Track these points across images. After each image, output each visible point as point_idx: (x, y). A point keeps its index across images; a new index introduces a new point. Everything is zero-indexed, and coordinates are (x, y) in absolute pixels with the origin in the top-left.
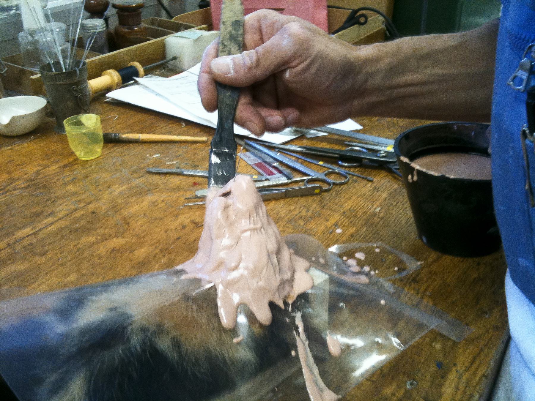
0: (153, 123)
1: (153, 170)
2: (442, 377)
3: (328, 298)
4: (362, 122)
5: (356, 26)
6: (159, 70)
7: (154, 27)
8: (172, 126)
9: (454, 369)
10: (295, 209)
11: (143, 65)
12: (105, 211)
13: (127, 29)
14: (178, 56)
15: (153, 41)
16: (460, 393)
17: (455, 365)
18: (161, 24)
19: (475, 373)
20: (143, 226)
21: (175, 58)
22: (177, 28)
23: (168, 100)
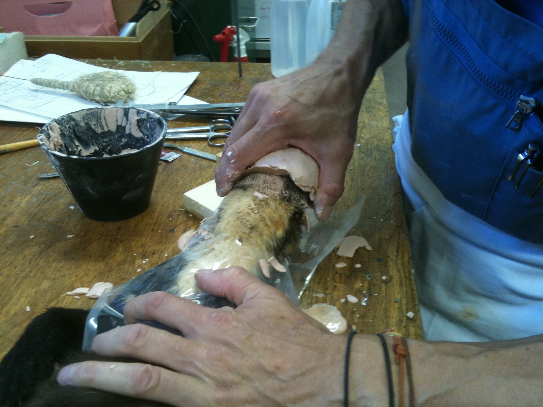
1: (45, 176)
2: (386, 266)
5: (151, 12)
8: (17, 132)
12: (26, 223)
16: (402, 272)
17: (388, 257)
23: (9, 108)
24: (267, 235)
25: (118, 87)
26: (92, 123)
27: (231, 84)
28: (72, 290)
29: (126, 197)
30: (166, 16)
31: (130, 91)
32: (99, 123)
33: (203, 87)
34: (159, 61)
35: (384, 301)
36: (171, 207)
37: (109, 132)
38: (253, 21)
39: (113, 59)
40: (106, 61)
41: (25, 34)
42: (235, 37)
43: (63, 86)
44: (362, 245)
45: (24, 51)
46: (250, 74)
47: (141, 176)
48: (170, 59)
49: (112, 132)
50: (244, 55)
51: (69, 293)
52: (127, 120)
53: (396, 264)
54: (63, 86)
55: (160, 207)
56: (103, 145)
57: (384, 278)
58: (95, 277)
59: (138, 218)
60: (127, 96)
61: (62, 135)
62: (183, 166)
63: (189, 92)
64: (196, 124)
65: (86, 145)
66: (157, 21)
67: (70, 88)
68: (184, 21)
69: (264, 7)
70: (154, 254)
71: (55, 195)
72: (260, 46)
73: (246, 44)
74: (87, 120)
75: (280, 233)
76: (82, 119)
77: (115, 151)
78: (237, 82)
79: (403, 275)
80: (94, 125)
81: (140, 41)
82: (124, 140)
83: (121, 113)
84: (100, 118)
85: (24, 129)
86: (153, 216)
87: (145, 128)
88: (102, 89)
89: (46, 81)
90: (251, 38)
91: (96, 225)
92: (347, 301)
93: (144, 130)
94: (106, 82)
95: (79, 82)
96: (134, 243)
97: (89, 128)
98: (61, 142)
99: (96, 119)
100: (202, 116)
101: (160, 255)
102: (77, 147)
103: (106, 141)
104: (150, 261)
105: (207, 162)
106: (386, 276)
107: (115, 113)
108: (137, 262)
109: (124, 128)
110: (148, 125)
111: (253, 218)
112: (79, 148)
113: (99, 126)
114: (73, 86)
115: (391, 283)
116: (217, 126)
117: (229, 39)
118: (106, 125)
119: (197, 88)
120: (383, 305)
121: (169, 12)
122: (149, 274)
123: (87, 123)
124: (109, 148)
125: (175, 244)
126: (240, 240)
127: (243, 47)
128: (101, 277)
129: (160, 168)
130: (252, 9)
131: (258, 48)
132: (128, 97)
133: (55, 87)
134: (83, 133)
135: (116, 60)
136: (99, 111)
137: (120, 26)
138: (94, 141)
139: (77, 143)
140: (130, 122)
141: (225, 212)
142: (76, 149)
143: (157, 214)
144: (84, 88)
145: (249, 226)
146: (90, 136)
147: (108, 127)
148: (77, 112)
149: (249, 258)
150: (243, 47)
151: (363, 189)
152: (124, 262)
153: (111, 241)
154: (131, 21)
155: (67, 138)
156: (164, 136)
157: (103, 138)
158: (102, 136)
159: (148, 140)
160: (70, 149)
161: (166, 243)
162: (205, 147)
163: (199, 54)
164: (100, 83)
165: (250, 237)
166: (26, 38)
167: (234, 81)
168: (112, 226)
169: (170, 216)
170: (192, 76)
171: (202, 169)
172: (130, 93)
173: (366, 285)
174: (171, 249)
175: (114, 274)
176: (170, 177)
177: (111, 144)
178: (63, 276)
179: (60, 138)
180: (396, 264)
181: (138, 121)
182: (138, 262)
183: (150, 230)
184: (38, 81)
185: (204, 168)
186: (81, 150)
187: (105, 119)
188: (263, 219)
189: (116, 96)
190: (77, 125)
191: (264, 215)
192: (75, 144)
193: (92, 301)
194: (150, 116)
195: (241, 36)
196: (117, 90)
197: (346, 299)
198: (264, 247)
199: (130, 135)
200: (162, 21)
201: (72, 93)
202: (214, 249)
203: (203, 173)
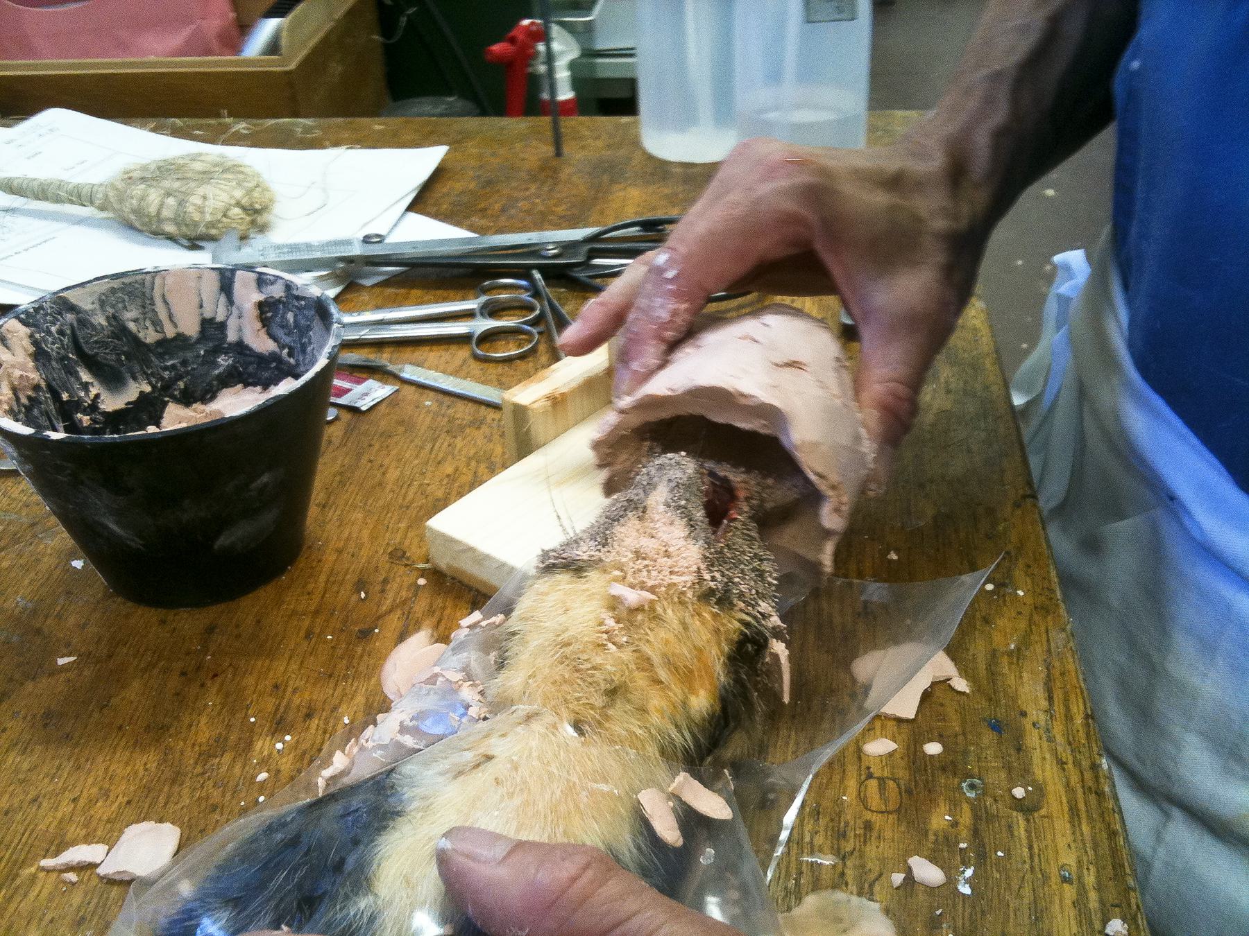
3: (529, 119)
4: (468, 222)
9: (1027, 723)
10: (457, 469)
13: (266, 485)
19: (1069, 717)
24: (662, 712)
25: (224, 197)
26: (130, 316)
27: (533, 178)
28: (57, 853)
29: (223, 541)
31: (257, 206)
32: (150, 315)
33: (458, 186)
34: (340, 120)
35: (1028, 876)
36: (364, 553)
37: (181, 339)
39: (218, 116)
42: (541, 47)
43: (79, 196)
44: (941, 675)
46: (583, 147)
47: (265, 478)
48: (374, 111)
50: (565, 94)
51: (48, 862)
52: (231, 302)
53: (1051, 740)
54: (79, 196)
55: (333, 557)
56: (162, 379)
57: (1019, 792)
58: (129, 802)
59: (265, 594)
60: (248, 219)
61: (40, 355)
62: (402, 423)
63: (422, 202)
64: (439, 292)
65: (113, 380)
67: (98, 202)
68: (410, 12)
70: (309, 716)
71: (33, 525)
72: (607, 68)
73: (572, 66)
74: (113, 306)
75: (701, 702)
76: (97, 306)
77: (198, 394)
78: (548, 172)
79: (1075, 779)
80: (136, 321)
82: (224, 361)
83: (211, 284)
84: (152, 299)
86: (310, 587)
87: (282, 327)
88: (181, 203)
90: (583, 50)
91: (144, 617)
92: (910, 879)
93: (280, 333)
94: (193, 184)
95: (120, 185)
96: (250, 681)
97: (120, 331)
98: (35, 376)
99: (139, 302)
100: (456, 271)
101: (327, 723)
102: (86, 386)
103: (173, 366)
104: (298, 742)
105: (471, 407)
106: (1024, 786)
108: (258, 745)
109: (222, 326)
110: (290, 316)
111: (613, 661)
112: (94, 391)
113: (148, 323)
114: (106, 197)
115: (1043, 812)
116: (497, 301)
117: (527, 55)
118: (170, 317)
119: (442, 189)
120: (1027, 892)
122: (279, 836)
123: (114, 317)
124: (181, 384)
125: (373, 681)
126: (577, 726)
127: (563, 75)
128: (146, 808)
129: (333, 433)
131: (602, 74)
132: (253, 222)
133: (58, 200)
135: (228, 120)
136: (148, 277)
137: (244, 28)
138: (137, 368)
139: (85, 376)
140: (238, 308)
141: (524, 642)
142: (82, 394)
143: (323, 578)
145: (603, 686)
146: (124, 353)
148: (82, 285)
149: (605, 788)
150: (563, 75)
151: (922, 486)
152: (218, 746)
153: (183, 674)
154: (270, 14)
155: (54, 363)
156: (333, 358)
157: (161, 356)
159: (292, 361)
160: (65, 396)
161: (346, 677)
162: (465, 361)
163: (450, 95)
164: (177, 185)
165: (607, 718)
167: (542, 169)
168: (188, 622)
169: (360, 585)
170: (422, 161)
171: (454, 429)
172: (257, 212)
173: (966, 818)
174: (360, 699)
175: (186, 792)
176: (364, 460)
177: (187, 373)
178: (35, 800)
179: (31, 364)
180: (1051, 740)
181: (261, 306)
182: (262, 746)
183: (302, 634)
184: (15, 183)
185: (462, 428)
186: (97, 396)
187: (165, 302)
188: (645, 663)
189: (219, 221)
190: (83, 322)
191: (647, 650)
192: (78, 378)
193: (115, 892)
194: (295, 292)
195: (556, 46)
196: (220, 205)
197: (909, 871)
198: (652, 751)
199: (240, 348)
201: (104, 215)
202: (489, 758)
203: (459, 442)
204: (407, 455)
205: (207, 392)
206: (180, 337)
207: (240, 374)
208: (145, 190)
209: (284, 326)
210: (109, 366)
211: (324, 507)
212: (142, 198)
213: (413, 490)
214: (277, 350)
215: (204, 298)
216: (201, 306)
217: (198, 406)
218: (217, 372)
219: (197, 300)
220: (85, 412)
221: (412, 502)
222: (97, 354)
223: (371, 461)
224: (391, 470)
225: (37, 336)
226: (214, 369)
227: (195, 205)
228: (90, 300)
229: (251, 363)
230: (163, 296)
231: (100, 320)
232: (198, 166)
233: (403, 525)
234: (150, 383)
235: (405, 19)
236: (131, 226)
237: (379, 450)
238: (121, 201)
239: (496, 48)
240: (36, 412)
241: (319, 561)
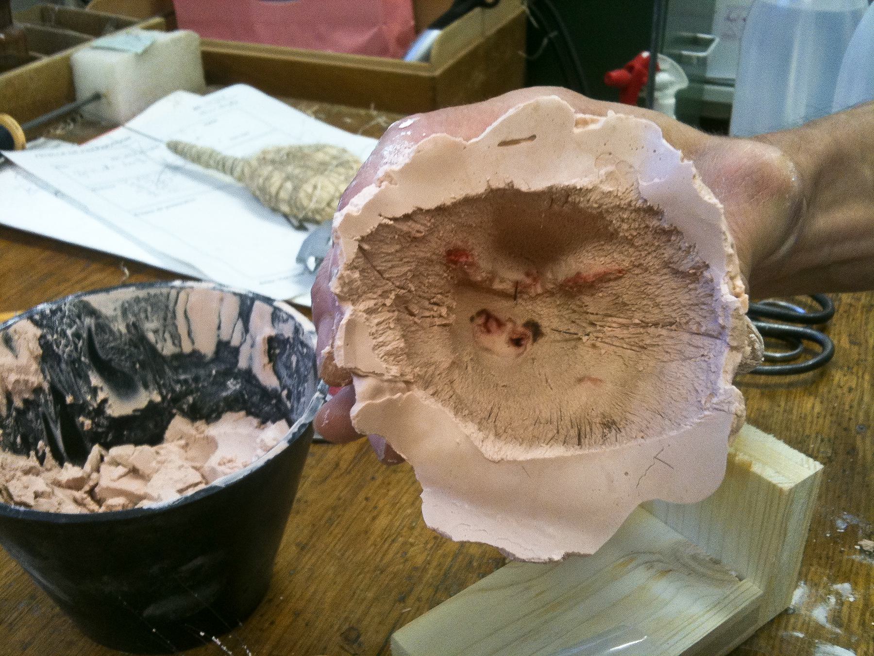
0: (50, 274)
5: (477, 10)
6: (62, 125)
7: (48, 29)
11: (21, 121)
14: (102, 90)
15: (45, 60)
18: (63, 20)
20: (30, 643)
21: (97, 97)
22: (97, 28)
25: (331, 189)
26: (150, 327)
30: (515, 21)
32: (170, 328)
37: (196, 357)
38: (705, 44)
39: (367, 106)
40: (354, 111)
41: (202, 36)
43: (224, 165)
45: (197, 73)
47: (198, 561)
49: (204, 356)
52: (246, 330)
56: (173, 391)
61: (48, 356)
65: (123, 385)
66: (491, 31)
69: (733, 16)
72: (712, 93)
74: (135, 315)
76: (119, 313)
77: (205, 411)
80: (156, 332)
81: (438, 73)
82: (233, 386)
83: (231, 308)
84: (174, 312)
85: (94, 266)
88: (296, 189)
89: (194, 150)
93: (284, 373)
95: (254, 163)
97: (138, 339)
99: (162, 314)
102: (94, 391)
103: (186, 381)
107: (215, 305)
109: (236, 351)
110: (294, 359)
112: (101, 396)
113: (167, 336)
118: (189, 333)
121: (524, 12)
123: (134, 324)
124: (190, 399)
130: (706, 20)
131: (707, 98)
133: (207, 166)
134: (120, 351)
135: (374, 113)
138: (150, 377)
139: (95, 380)
144: (261, 181)
147: (193, 343)
155: (63, 366)
157: (176, 370)
158: (175, 364)
159: (289, 405)
160: (69, 399)
164: (297, 171)
166: (203, 44)
177: (197, 390)
179: (34, 366)
186: (105, 401)
189: (323, 210)
190: (102, 326)
192: (88, 382)
199: (248, 376)
200: (502, 33)
204: (404, 500)
205: (213, 411)
206: (195, 353)
207: (245, 402)
208: (271, 172)
209: (288, 367)
210: (124, 374)
211: (303, 549)
212: (268, 178)
213: (396, 546)
214: (279, 389)
215: (223, 319)
216: (219, 328)
217: (201, 424)
218: (224, 394)
219: (217, 322)
220: (88, 415)
221: (388, 565)
222: (111, 360)
223: (367, 499)
224: (381, 517)
225: (49, 337)
226: (223, 390)
227: (306, 192)
228: (112, 307)
229: (255, 394)
230: (185, 312)
231: (120, 327)
232: (320, 156)
233: (370, 595)
234: (161, 393)
235: (545, 41)
236: (257, 199)
237: (379, 487)
238: (252, 177)
239: (615, 74)
240: (31, 415)
241: (272, 623)
